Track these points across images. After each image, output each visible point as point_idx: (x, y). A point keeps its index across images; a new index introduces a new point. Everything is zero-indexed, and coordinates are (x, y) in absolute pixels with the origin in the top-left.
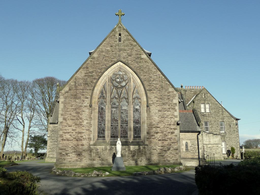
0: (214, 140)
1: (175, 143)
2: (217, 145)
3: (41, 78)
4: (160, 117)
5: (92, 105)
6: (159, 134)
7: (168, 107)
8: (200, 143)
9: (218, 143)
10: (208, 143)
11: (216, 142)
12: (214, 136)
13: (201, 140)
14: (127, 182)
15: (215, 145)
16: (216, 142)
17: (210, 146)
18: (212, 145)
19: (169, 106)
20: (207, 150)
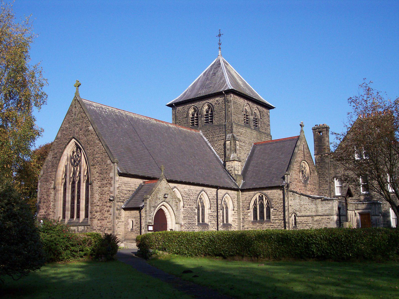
0: (324, 208)
1: (109, 222)
2: (327, 217)
3: (321, 124)
4: (100, 194)
5: (56, 187)
6: (98, 213)
7: (106, 182)
8: (142, 221)
9: (329, 213)
10: (314, 214)
11: (327, 212)
12: (324, 202)
13: (144, 218)
14: (84, 265)
15: (324, 217)
16: (327, 212)
17: (317, 218)
18: (321, 217)
19: (107, 181)
20: (313, 224)
